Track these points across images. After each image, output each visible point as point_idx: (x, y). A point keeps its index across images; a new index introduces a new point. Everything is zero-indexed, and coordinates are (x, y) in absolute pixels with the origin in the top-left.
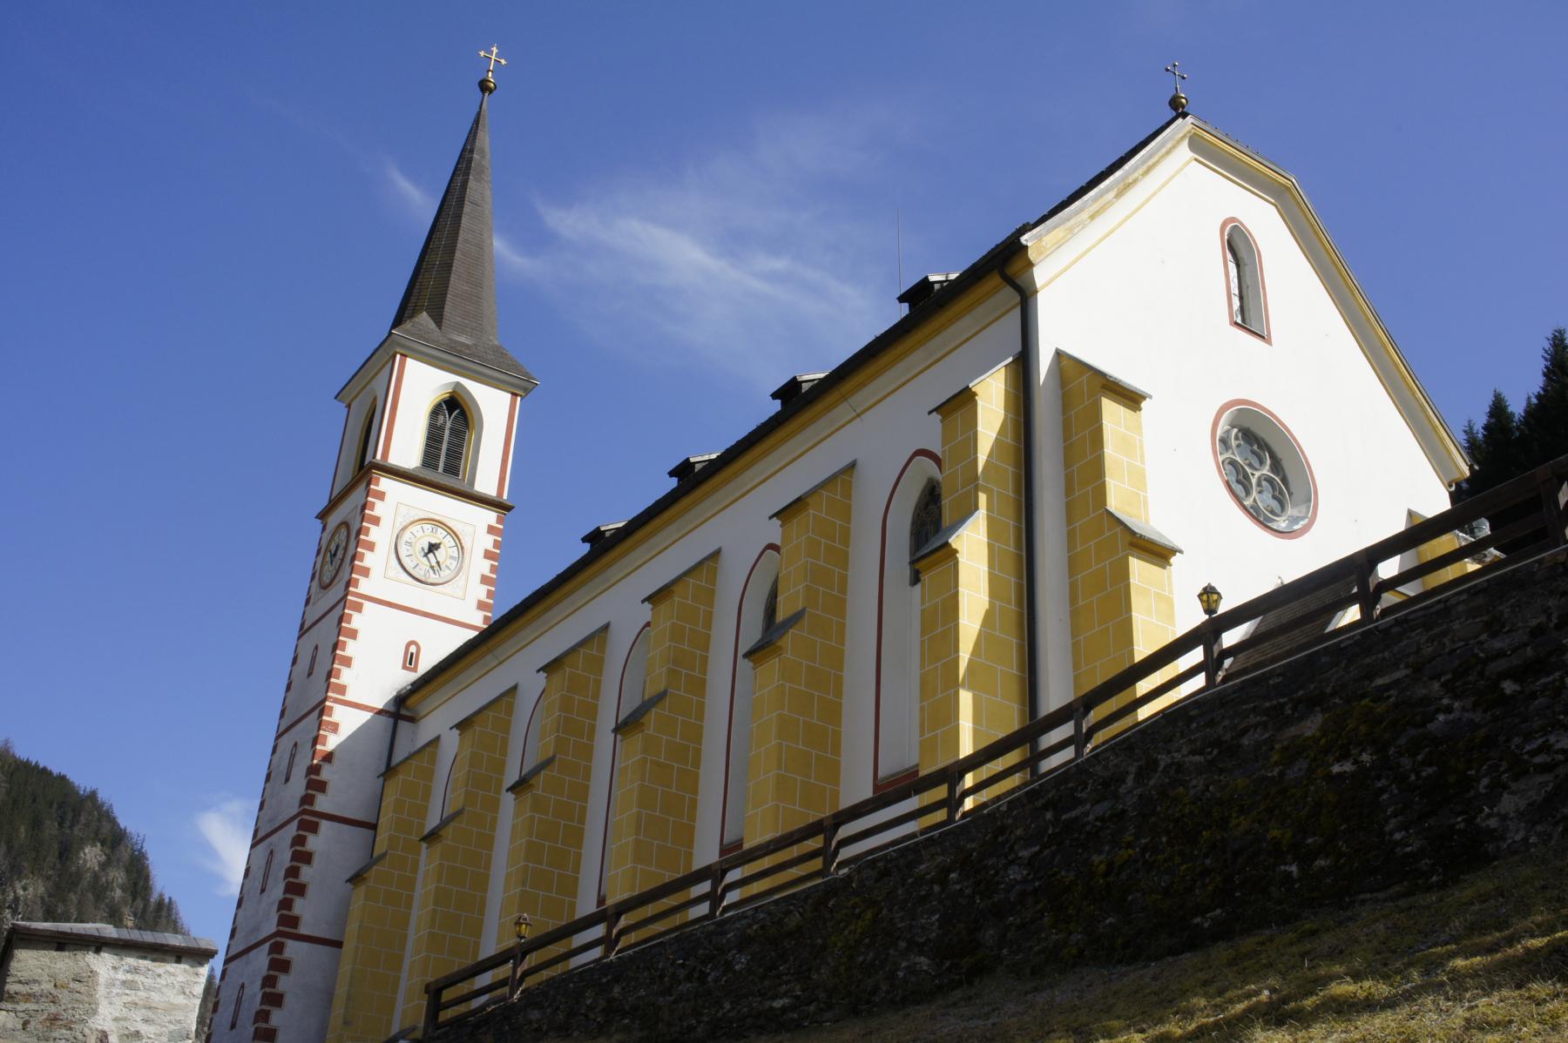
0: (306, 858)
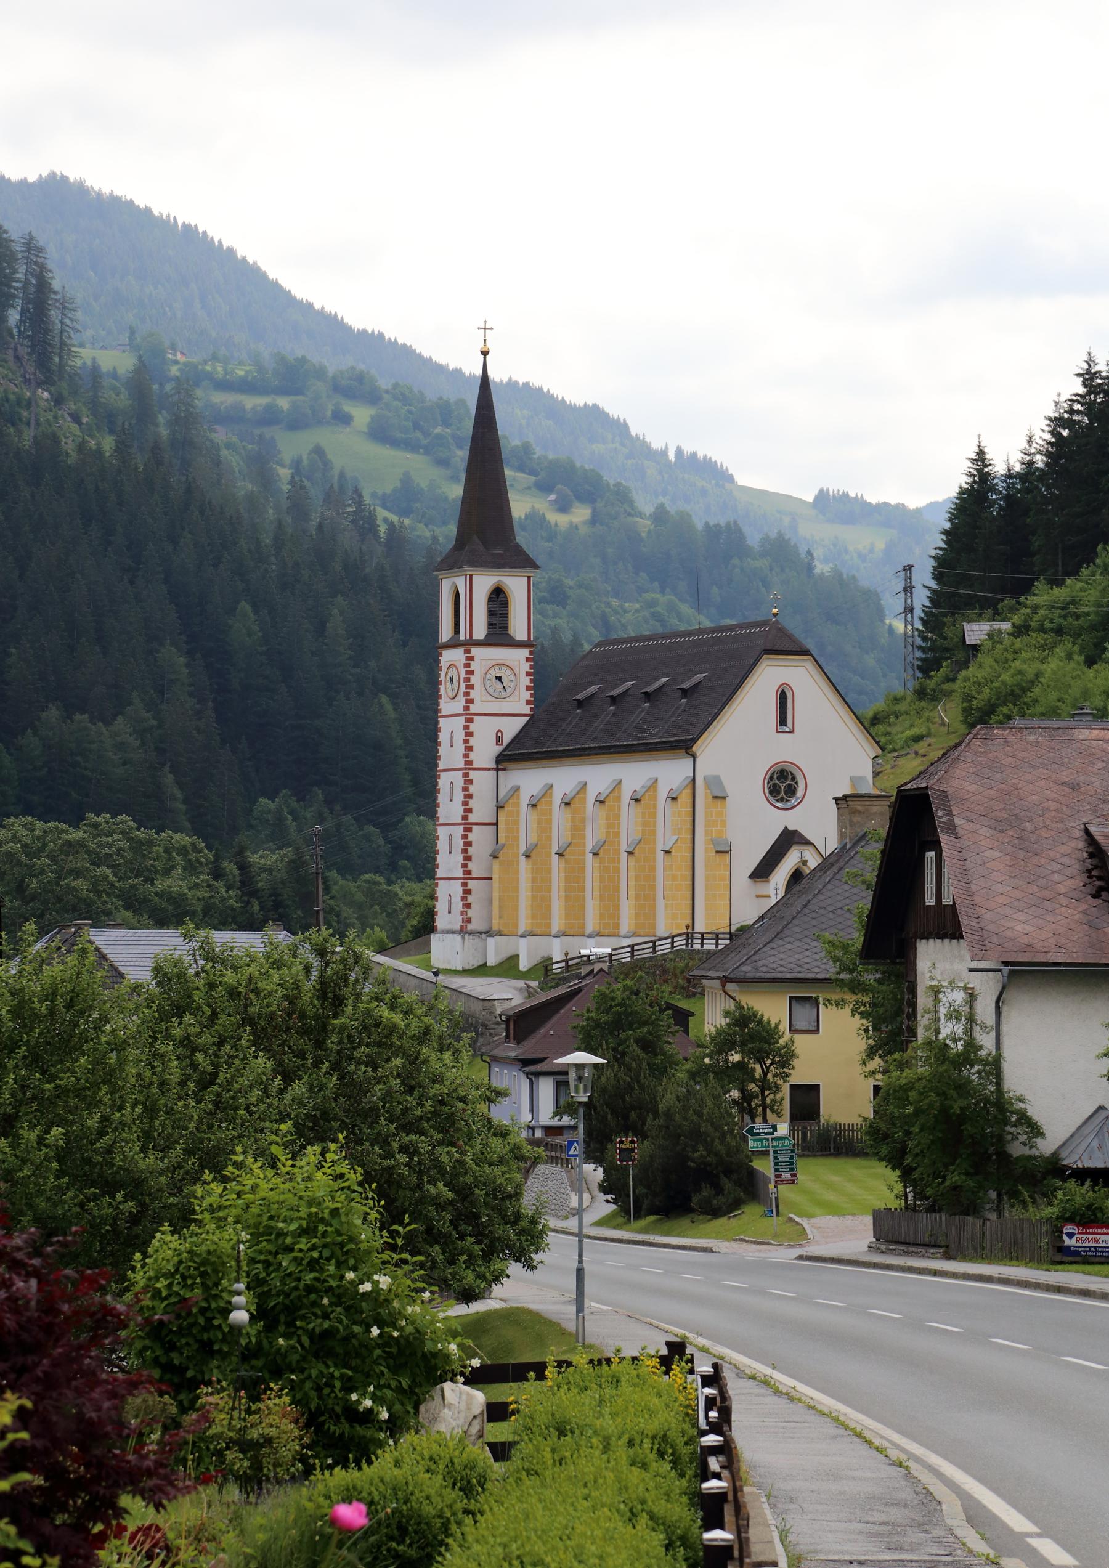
0: (469, 844)
